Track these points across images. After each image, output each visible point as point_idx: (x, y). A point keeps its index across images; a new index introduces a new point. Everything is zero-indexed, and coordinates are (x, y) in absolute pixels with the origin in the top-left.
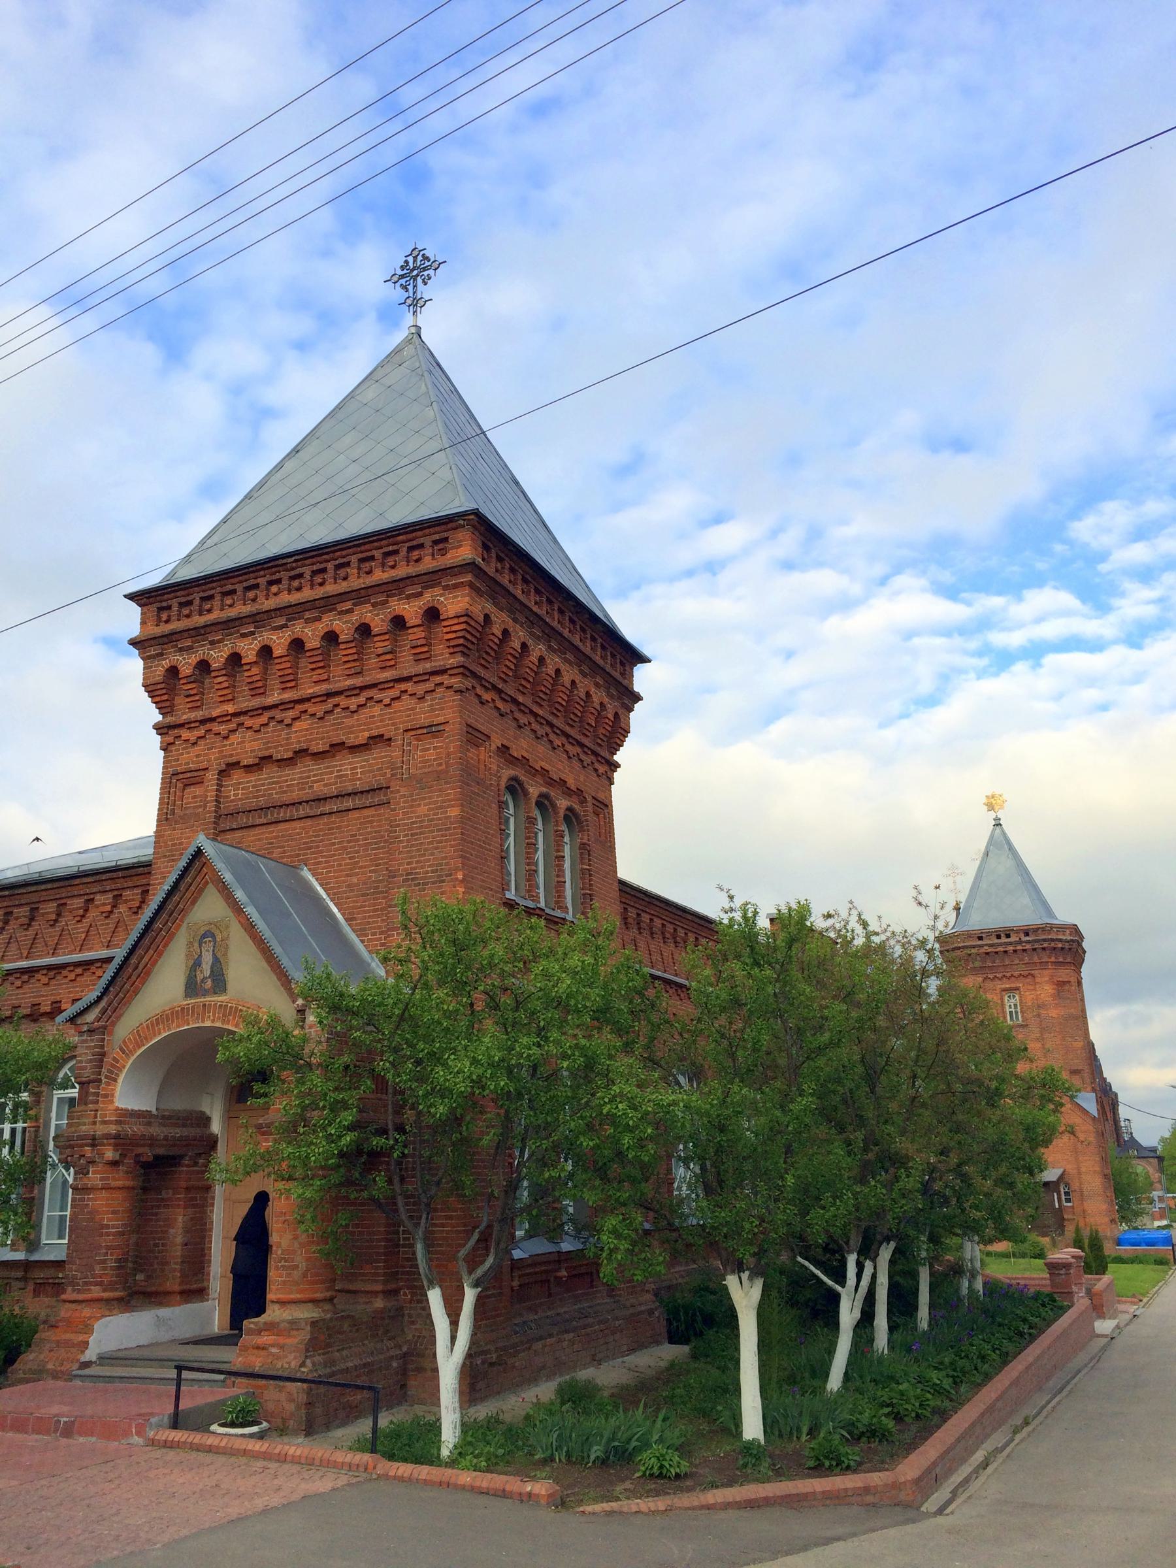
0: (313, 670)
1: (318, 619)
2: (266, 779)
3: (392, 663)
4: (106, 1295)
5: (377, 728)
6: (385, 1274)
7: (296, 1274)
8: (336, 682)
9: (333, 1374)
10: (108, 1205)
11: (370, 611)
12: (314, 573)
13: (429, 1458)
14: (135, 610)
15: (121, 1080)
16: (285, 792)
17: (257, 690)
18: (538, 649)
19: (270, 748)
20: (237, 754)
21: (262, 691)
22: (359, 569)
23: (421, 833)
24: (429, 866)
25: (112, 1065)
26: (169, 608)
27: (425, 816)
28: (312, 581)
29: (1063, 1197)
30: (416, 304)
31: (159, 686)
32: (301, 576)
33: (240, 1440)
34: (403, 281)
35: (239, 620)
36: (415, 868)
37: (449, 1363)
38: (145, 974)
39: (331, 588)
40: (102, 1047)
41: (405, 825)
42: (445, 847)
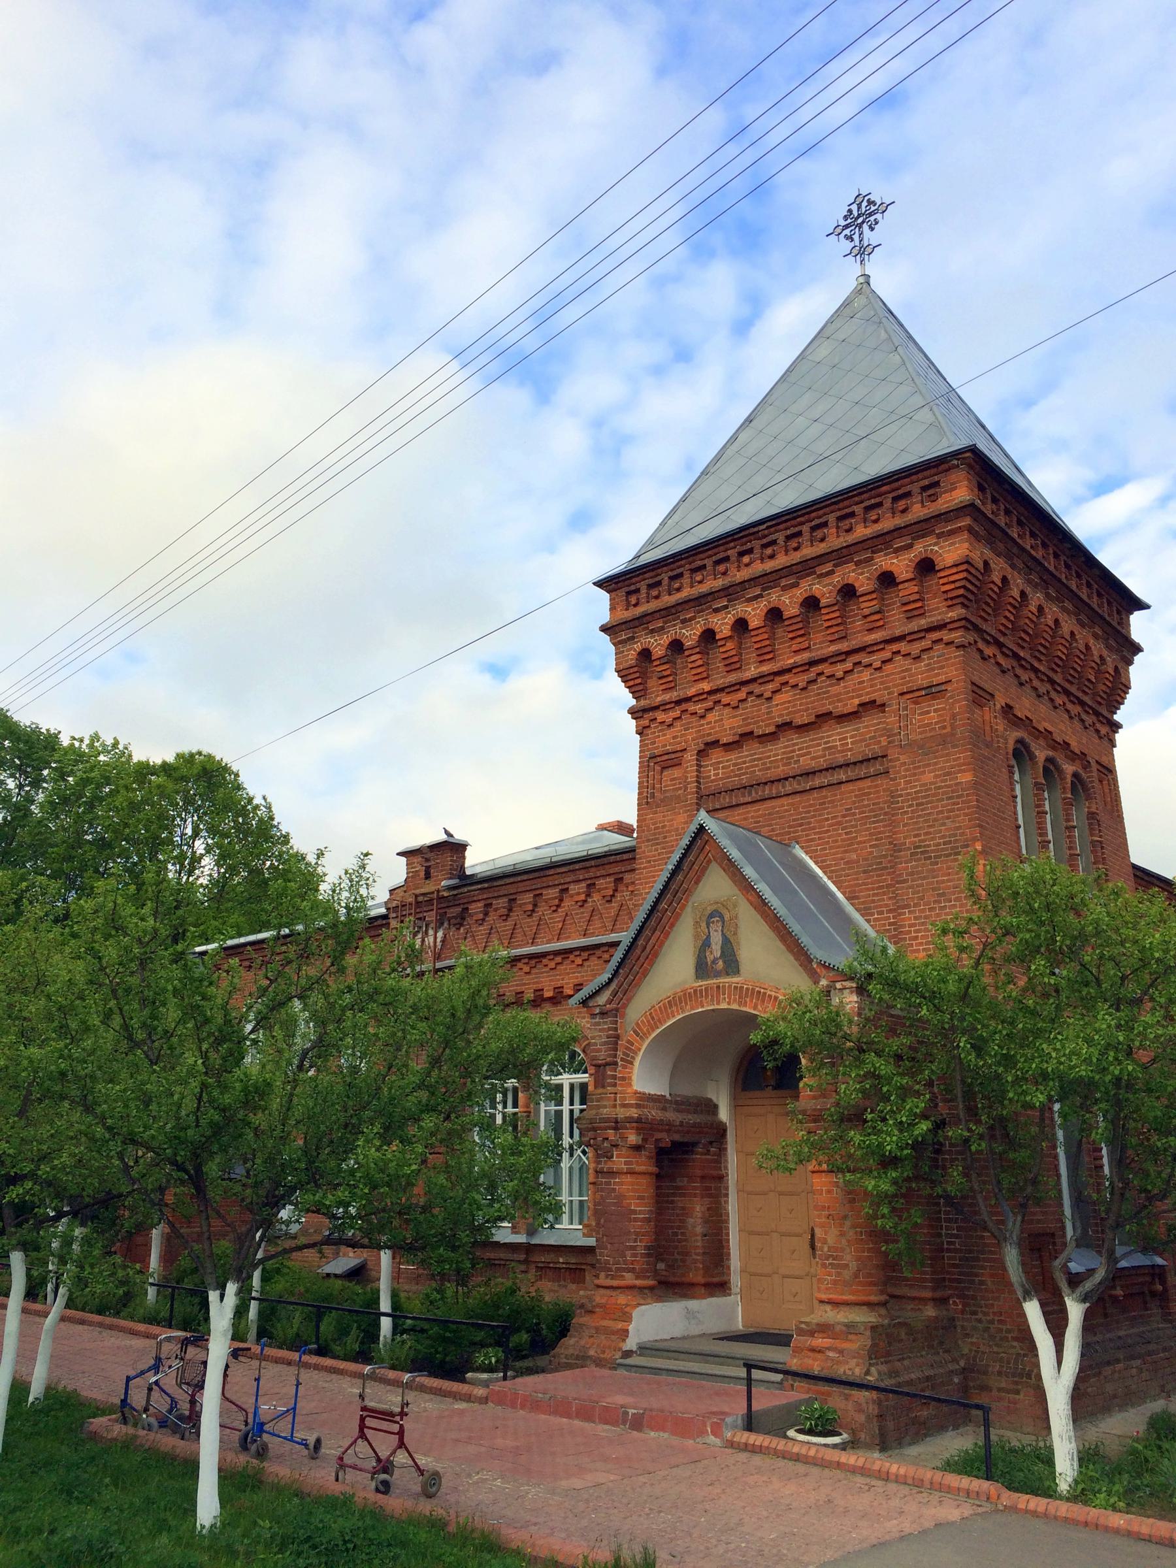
0: (792, 639)
1: (795, 585)
2: (747, 756)
3: (881, 623)
4: (638, 1282)
5: (868, 693)
6: (932, 1280)
7: (847, 1274)
8: (818, 649)
9: (899, 1385)
10: (634, 1190)
11: (854, 571)
12: (788, 538)
13: (1049, 1492)
14: (604, 597)
15: (637, 1063)
16: (769, 768)
17: (732, 666)
18: (1036, 598)
19: (750, 724)
20: (716, 733)
21: (738, 665)
22: (838, 527)
23: (927, 803)
24: (940, 838)
25: (627, 1048)
26: (637, 591)
27: (931, 783)
28: (786, 546)
29: (815, 1287)
30: (862, 252)
31: (632, 671)
32: (774, 542)
33: (830, 1451)
34: (847, 232)
35: (712, 595)
36: (924, 841)
37: (1058, 1384)
38: (653, 956)
39: (808, 551)
40: (616, 1029)
41: (908, 794)
42: (958, 816)
